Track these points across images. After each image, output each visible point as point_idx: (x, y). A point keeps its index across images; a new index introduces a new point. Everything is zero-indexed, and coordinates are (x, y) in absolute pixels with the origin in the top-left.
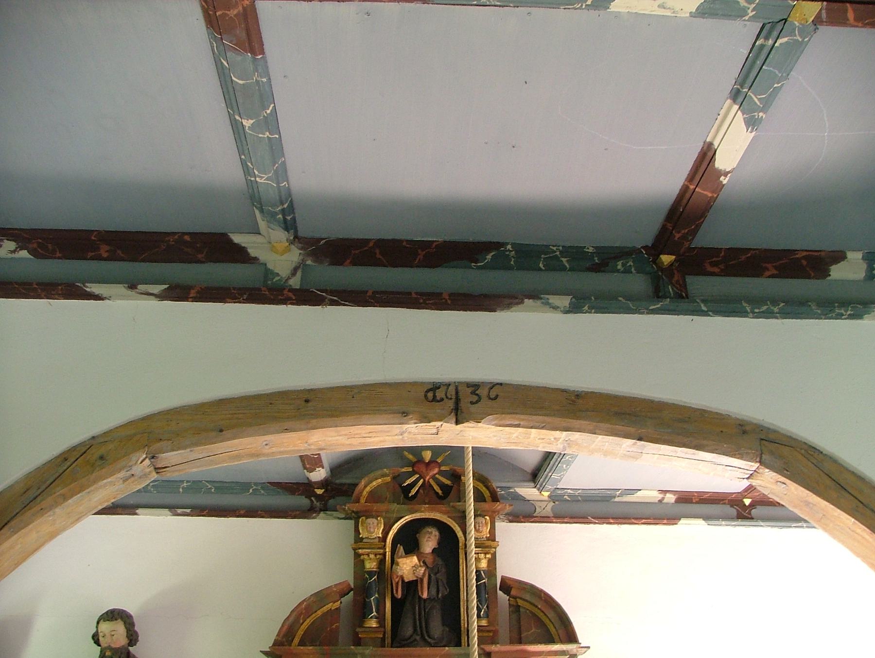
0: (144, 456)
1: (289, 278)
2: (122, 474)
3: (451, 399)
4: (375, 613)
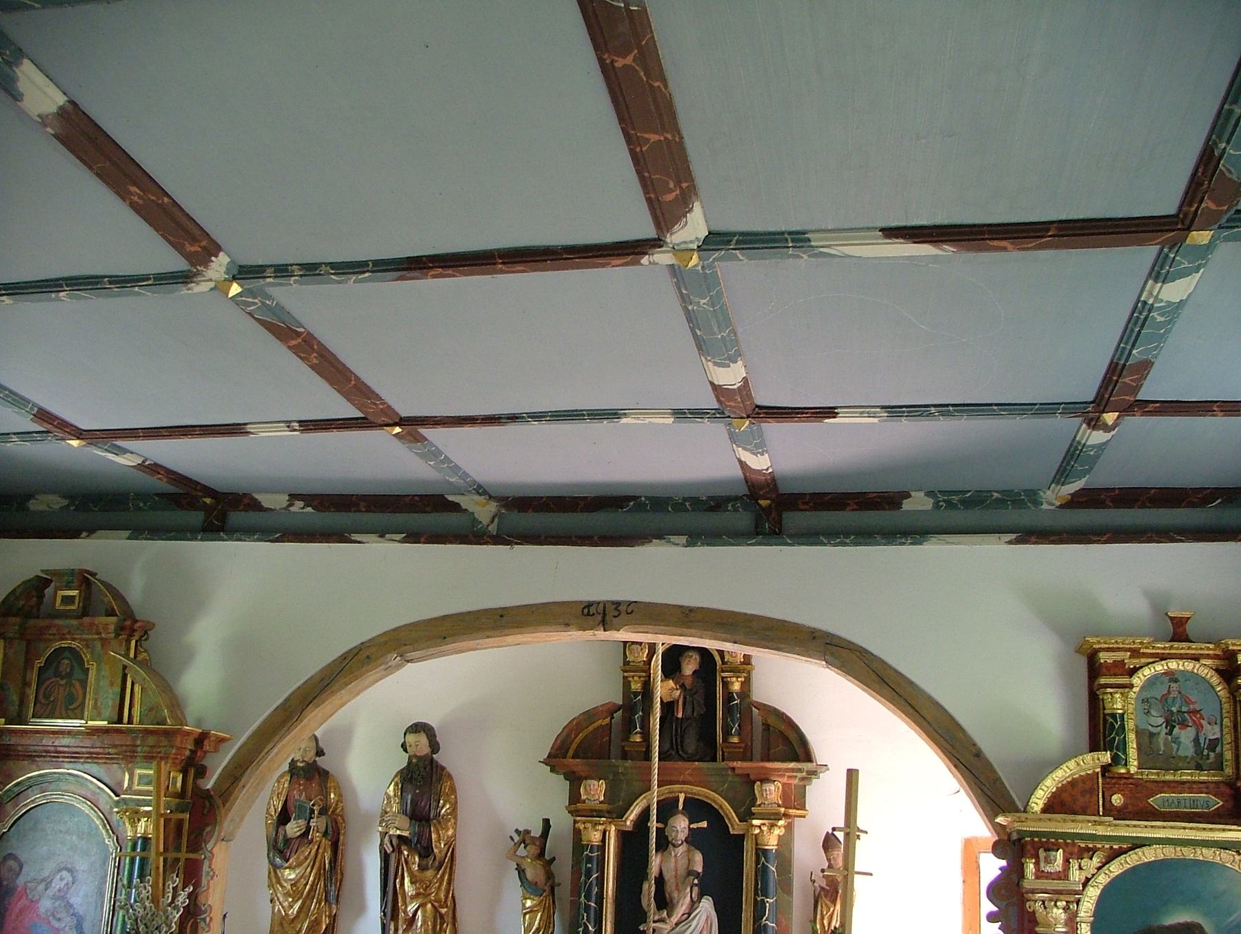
0: (396, 655)
1: (488, 526)
2: (383, 667)
3: (600, 614)
4: (638, 729)
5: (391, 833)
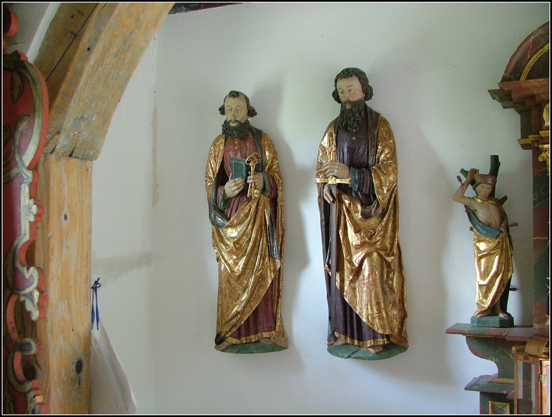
5: (329, 183)
